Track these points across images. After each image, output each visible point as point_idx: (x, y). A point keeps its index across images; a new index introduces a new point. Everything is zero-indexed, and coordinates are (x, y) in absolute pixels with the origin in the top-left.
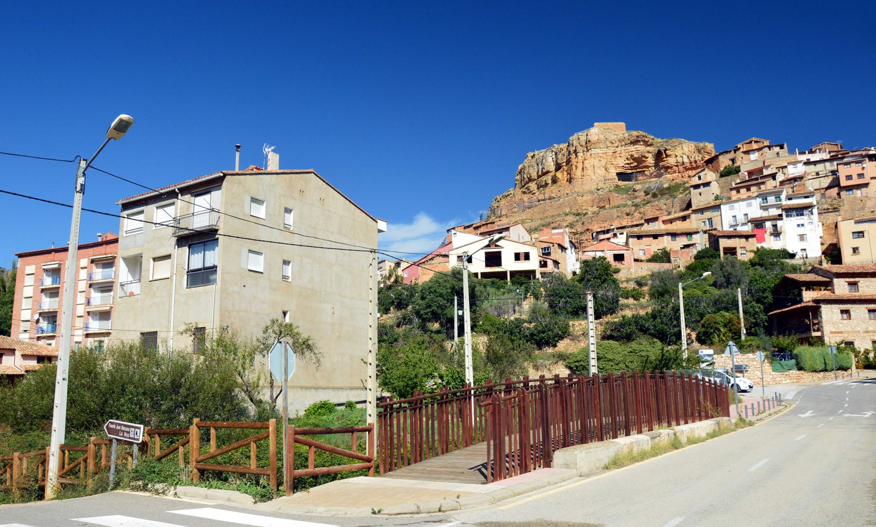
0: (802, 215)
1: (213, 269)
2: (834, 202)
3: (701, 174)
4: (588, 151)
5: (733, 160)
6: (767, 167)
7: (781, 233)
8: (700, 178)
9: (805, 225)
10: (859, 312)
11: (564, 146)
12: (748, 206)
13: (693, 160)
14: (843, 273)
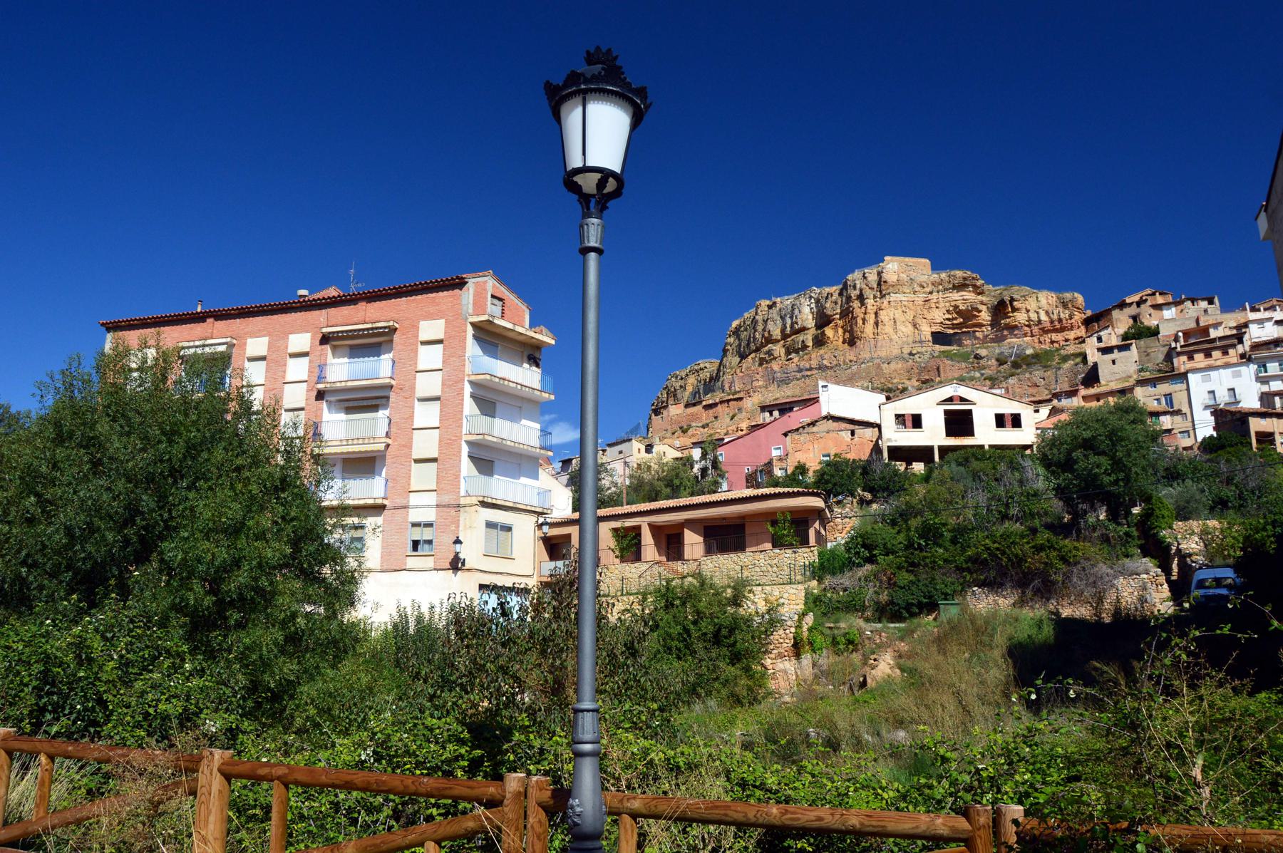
3: (1101, 333)
4: (883, 296)
11: (835, 290)
12: (1234, 377)
13: (1055, 317)
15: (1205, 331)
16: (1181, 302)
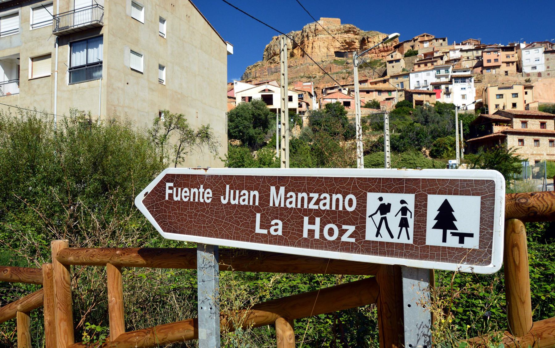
0: (465, 82)
1: (98, 65)
2: (479, 76)
3: (393, 54)
4: (316, 36)
5: (413, 47)
6: (437, 52)
7: (450, 93)
8: (392, 57)
9: (466, 89)
10: (544, 141)
11: (299, 32)
12: (427, 75)
14: (520, 115)
15: (432, 54)
16: (431, 40)
